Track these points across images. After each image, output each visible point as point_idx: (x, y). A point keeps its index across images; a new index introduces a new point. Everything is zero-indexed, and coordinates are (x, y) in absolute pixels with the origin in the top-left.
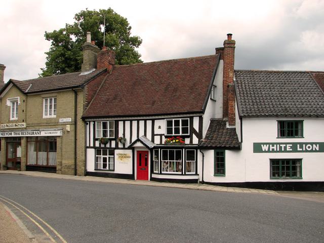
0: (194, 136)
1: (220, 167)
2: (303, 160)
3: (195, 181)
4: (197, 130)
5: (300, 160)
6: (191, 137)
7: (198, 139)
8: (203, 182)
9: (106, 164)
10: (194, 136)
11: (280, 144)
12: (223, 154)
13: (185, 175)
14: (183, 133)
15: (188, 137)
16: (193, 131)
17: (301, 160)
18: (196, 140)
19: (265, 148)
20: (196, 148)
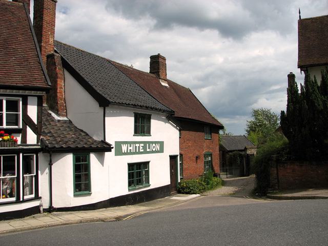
0: (29, 131)
1: (82, 182)
2: (150, 164)
3: (35, 211)
4: (35, 120)
5: (146, 164)
6: (23, 132)
7: (36, 136)
8: (51, 210)
9: (7, 110)
10: (29, 131)
11: (135, 143)
12: (87, 159)
13: (24, 201)
14: (8, 124)
15: (18, 131)
16: (27, 121)
17: (148, 163)
18: (32, 138)
19: (124, 148)
20: (36, 151)
